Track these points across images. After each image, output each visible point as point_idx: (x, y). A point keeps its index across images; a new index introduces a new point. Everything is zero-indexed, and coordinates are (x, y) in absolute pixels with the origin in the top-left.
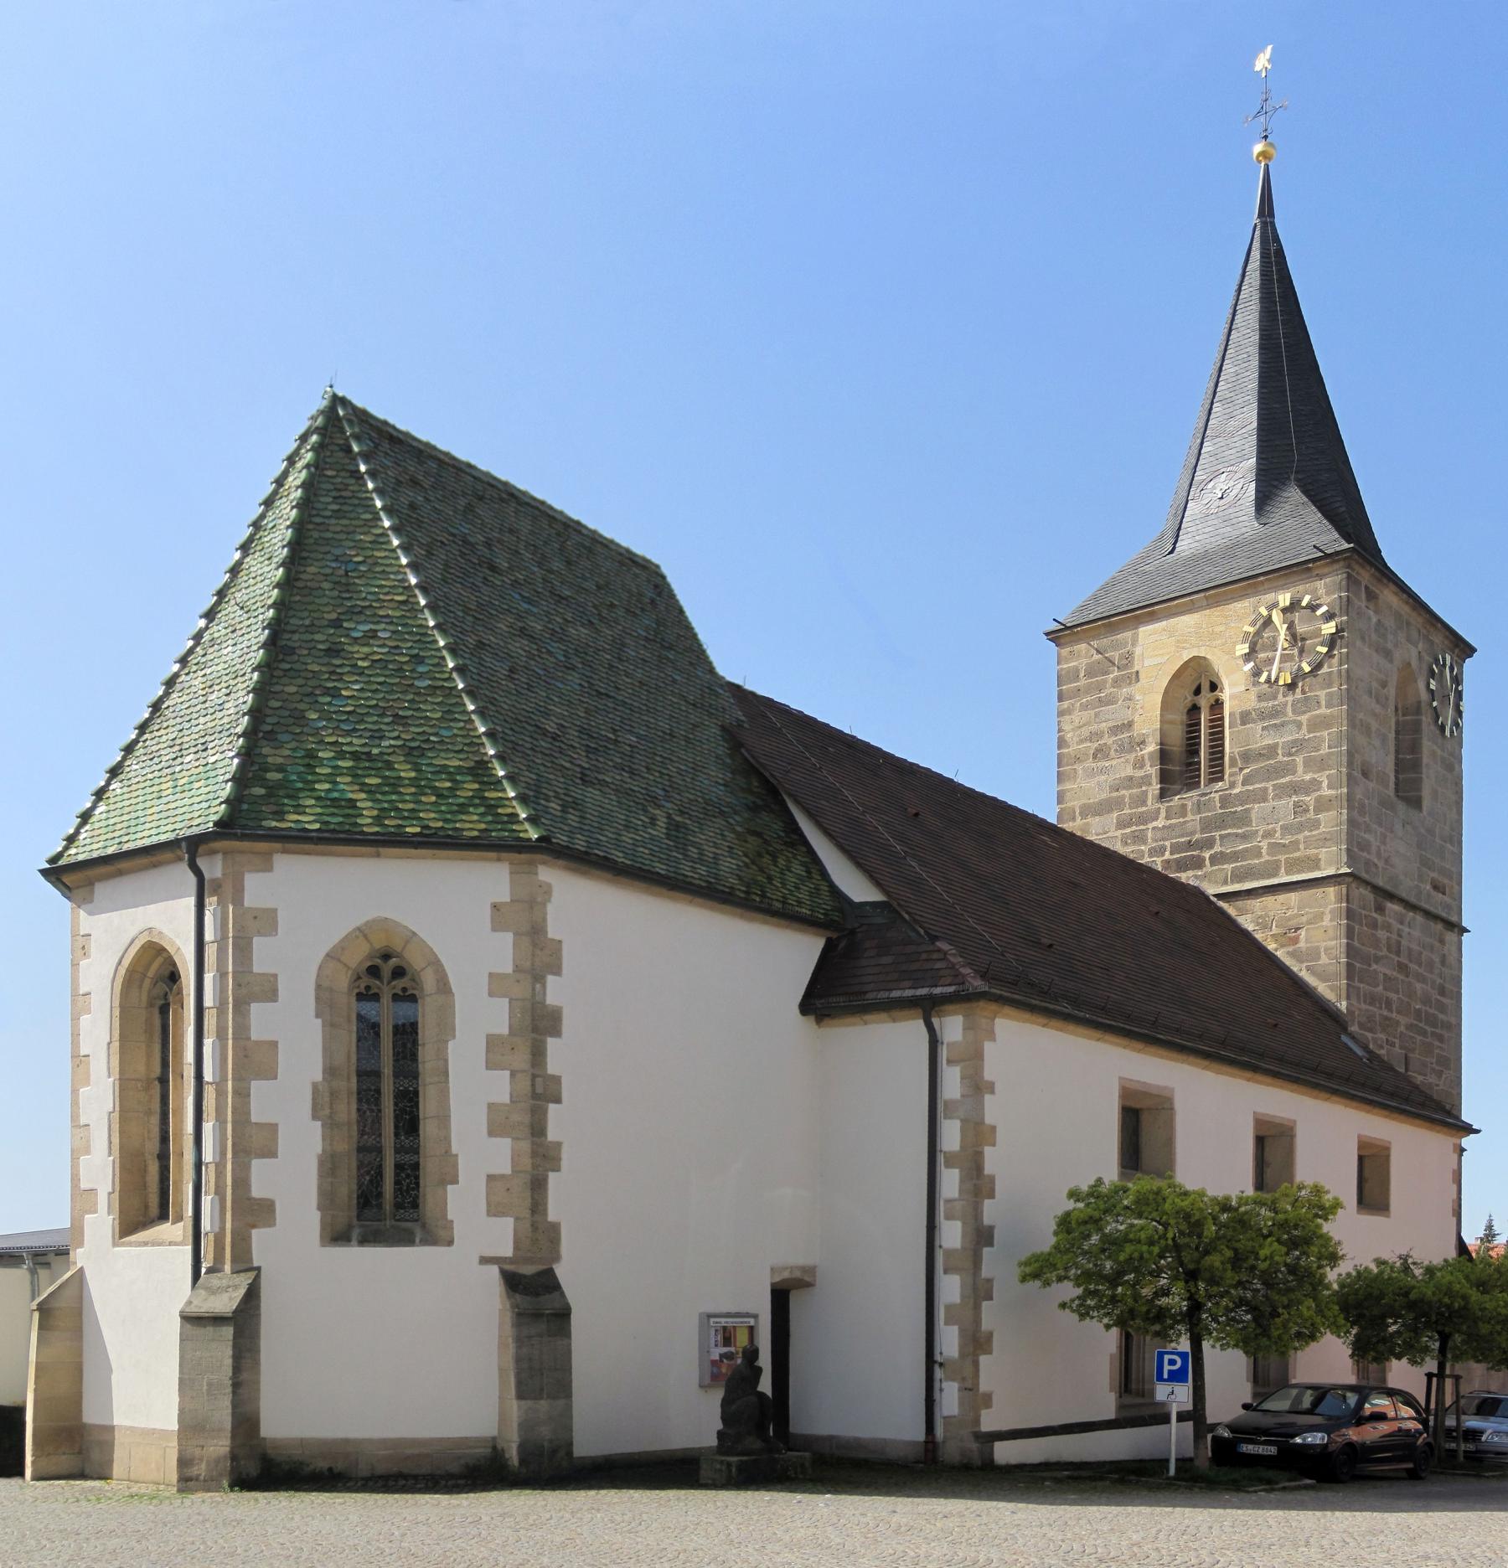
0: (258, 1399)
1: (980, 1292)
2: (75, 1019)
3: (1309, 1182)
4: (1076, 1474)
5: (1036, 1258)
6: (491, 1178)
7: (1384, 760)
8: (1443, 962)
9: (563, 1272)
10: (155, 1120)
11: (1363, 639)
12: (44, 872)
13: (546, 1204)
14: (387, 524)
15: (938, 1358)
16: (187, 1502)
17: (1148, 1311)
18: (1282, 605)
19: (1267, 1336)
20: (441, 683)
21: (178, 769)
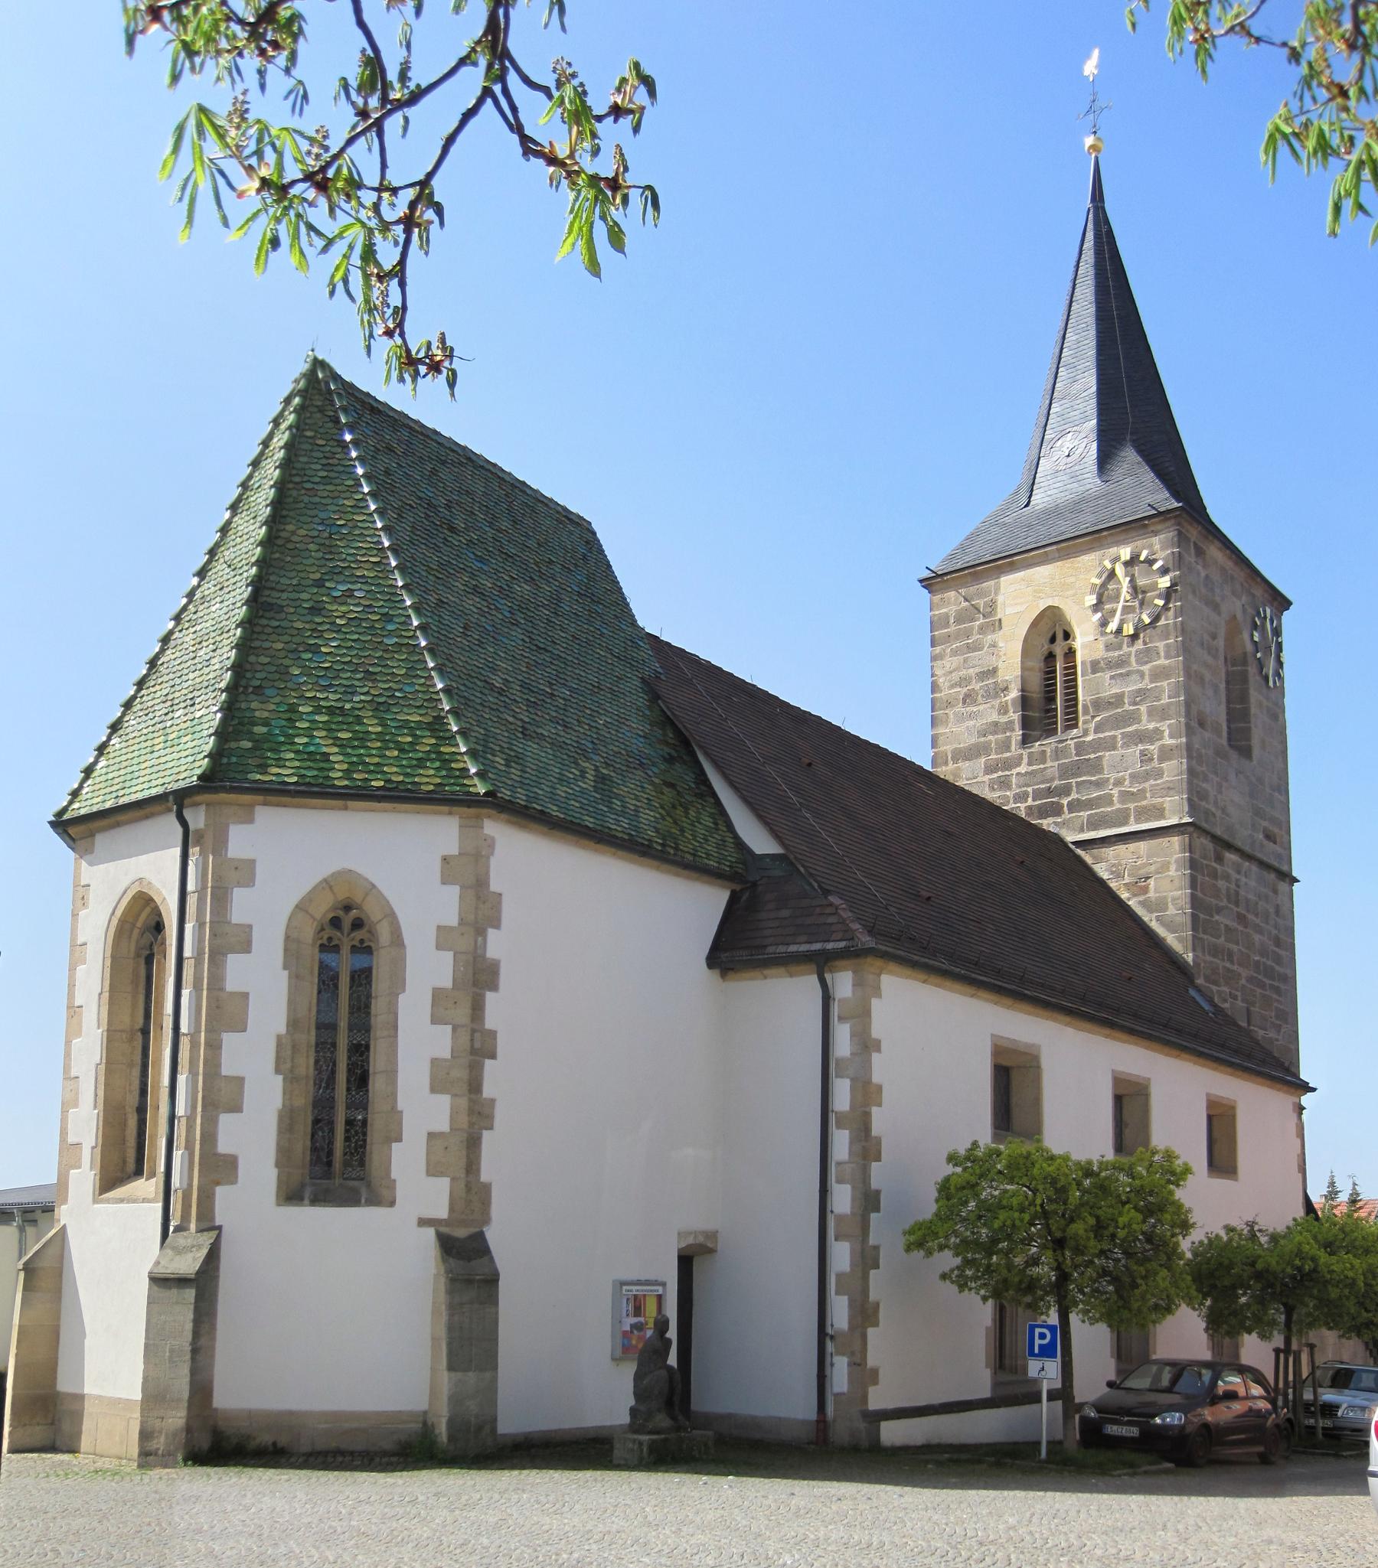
0: (211, 1366)
1: (867, 1259)
2: (72, 969)
3: (1161, 1147)
4: (955, 1456)
5: (919, 1226)
6: (431, 1136)
7: (1217, 710)
8: (1277, 912)
9: (493, 1236)
10: (136, 1072)
11: (1194, 592)
12: (51, 823)
13: (479, 1164)
14: (366, 490)
15: (829, 1330)
16: (146, 1479)
17: (1020, 1282)
18: (1123, 559)
19: (1129, 1314)
20: (406, 641)
21: (169, 724)
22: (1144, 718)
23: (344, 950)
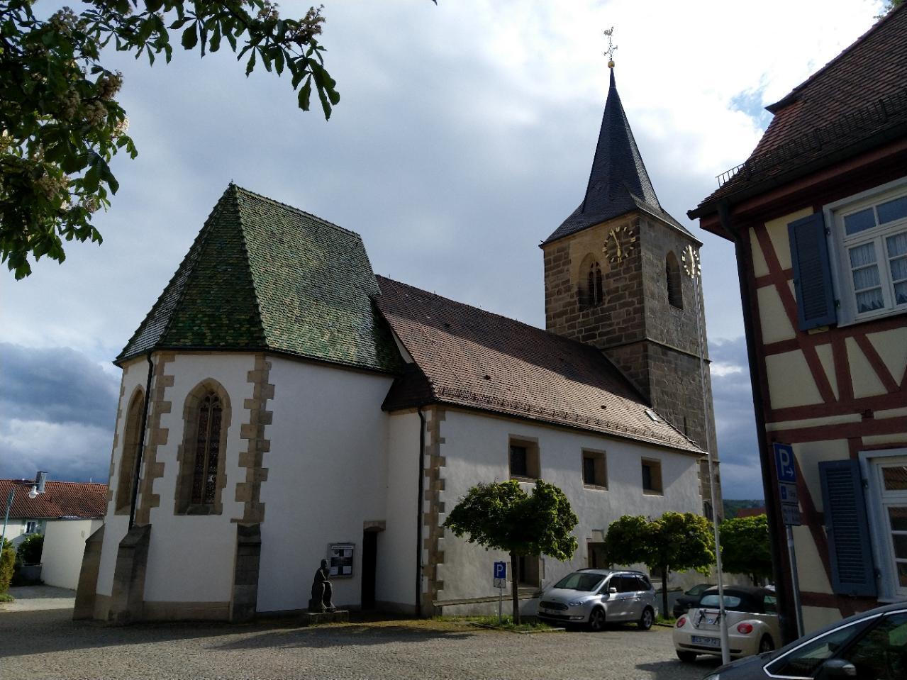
22: (627, 296)
23: (208, 408)
